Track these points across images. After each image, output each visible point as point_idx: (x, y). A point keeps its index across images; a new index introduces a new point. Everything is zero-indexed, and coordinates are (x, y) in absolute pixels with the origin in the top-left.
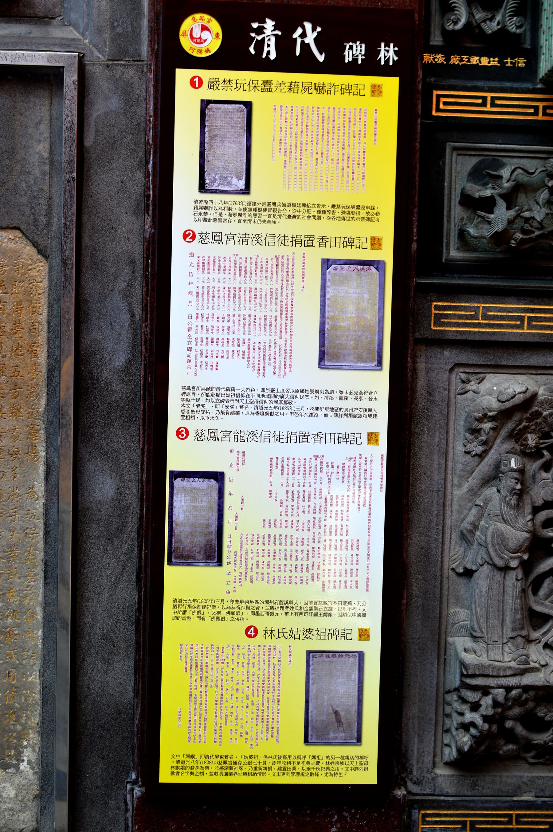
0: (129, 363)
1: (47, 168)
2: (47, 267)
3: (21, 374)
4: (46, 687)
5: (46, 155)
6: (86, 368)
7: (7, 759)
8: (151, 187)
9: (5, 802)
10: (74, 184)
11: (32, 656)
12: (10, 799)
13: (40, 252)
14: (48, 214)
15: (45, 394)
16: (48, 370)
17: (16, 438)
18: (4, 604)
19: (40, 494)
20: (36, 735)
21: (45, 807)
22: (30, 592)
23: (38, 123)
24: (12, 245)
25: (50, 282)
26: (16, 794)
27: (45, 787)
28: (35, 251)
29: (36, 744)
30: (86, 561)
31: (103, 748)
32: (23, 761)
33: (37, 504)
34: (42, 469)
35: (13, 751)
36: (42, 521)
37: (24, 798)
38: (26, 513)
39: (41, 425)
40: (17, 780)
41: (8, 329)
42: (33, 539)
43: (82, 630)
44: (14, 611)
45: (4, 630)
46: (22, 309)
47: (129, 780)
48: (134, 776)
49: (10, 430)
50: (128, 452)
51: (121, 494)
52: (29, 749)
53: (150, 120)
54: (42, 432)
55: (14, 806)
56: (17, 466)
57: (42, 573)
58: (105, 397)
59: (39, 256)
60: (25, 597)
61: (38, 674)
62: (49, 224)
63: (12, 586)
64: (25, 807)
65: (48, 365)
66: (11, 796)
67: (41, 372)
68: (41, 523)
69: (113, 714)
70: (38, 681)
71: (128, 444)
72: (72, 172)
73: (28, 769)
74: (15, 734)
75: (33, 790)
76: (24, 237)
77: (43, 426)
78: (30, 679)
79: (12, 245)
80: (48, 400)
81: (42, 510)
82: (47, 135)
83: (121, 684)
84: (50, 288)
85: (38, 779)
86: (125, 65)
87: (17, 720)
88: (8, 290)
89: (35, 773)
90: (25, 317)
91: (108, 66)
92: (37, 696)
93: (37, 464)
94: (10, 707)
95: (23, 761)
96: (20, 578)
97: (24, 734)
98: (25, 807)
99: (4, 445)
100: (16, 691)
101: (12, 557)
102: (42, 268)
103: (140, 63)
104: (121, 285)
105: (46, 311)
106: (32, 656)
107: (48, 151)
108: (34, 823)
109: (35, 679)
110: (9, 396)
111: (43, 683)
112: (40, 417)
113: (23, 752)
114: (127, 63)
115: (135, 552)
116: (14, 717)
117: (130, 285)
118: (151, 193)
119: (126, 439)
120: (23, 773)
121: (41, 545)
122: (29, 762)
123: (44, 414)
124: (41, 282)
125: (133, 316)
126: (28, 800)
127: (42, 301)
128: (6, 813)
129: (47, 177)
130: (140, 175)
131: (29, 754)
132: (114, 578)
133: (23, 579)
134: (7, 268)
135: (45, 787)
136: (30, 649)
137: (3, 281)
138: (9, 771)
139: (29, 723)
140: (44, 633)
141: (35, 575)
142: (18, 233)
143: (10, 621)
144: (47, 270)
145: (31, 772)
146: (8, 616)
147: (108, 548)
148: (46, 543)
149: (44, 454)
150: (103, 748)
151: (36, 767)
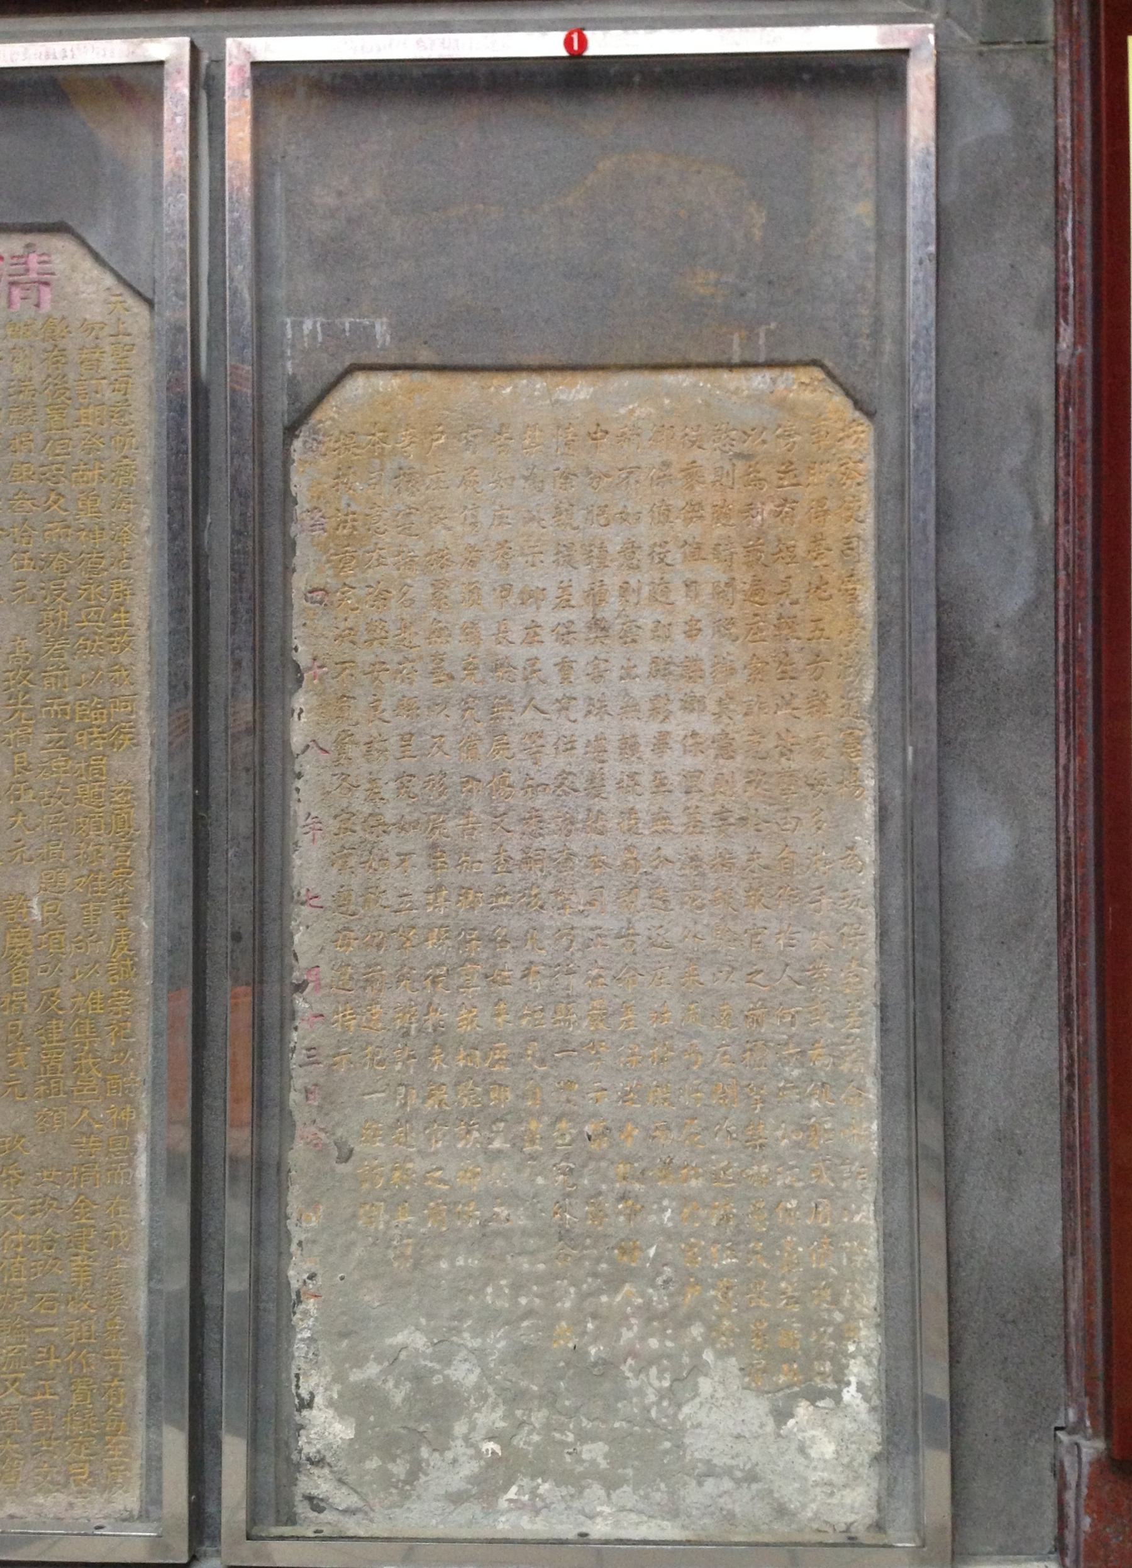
0: (1034, 605)
1: (871, 248)
2: (872, 434)
3: (826, 633)
4: (890, 1236)
5: (869, 223)
6: (949, 617)
7: (818, 1380)
8: (1071, 270)
9: (815, 1468)
10: (931, 267)
11: (859, 1173)
12: (825, 1461)
13: (858, 405)
14: (876, 334)
15: (873, 670)
16: (880, 623)
17: (819, 753)
18: (804, 1070)
19: (867, 860)
20: (873, 1331)
21: (895, 1479)
22: (853, 1047)
23: (854, 166)
24: (807, 395)
25: (879, 456)
26: (837, 1452)
27: (896, 1438)
28: (849, 404)
29: (873, 1350)
30: (958, 987)
31: (1006, 1359)
32: (848, 1384)
33: (863, 877)
34: (869, 811)
35: (828, 1363)
36: (872, 910)
37: (853, 1460)
38: (842, 895)
39: (866, 729)
40: (836, 1424)
41: (801, 551)
42: (855, 945)
43: (956, 1121)
44: (823, 1084)
45: (804, 1122)
46: (826, 512)
47: (1060, 1423)
48: (1072, 1415)
49: (808, 741)
50: (1035, 775)
51: (1022, 856)
52: (860, 1360)
53: (1065, 147)
54: (869, 741)
55: (833, 1477)
56: (823, 806)
57: (874, 1012)
58: (987, 672)
59: (857, 414)
60: (841, 1057)
61: (872, 1208)
62: (876, 352)
63: (817, 1036)
64: (856, 1478)
65: (879, 613)
66: (827, 1457)
67: (864, 628)
68: (870, 916)
69: (1023, 1290)
70: (872, 1222)
71: (1033, 759)
72: (927, 244)
73: (858, 1401)
74: (830, 1330)
75: (869, 1443)
76: (828, 380)
77: (870, 731)
78: (857, 1219)
79: (807, 395)
80: (880, 682)
81: (871, 889)
82: (870, 185)
83: (1037, 1229)
84: (879, 472)
85: (880, 1422)
86: (1011, 51)
87: (836, 1301)
88: (802, 479)
89: (873, 1409)
90: (832, 528)
91: (981, 54)
92: (872, 1253)
93: (860, 803)
94: (820, 1275)
95: (848, 1384)
96: (832, 1021)
97: (849, 1330)
98: (856, 1478)
99: (798, 767)
100: (831, 1244)
101: (816, 980)
102: (862, 436)
103: (1038, 46)
104: (1013, 459)
105: (872, 515)
106: (859, 1173)
107: (872, 215)
108: (873, 1512)
109: (869, 1219)
110: (805, 676)
111: (885, 1228)
112: (864, 714)
113: (847, 1366)
114: (1017, 47)
115: (1055, 968)
116: (827, 1294)
117: (1033, 457)
118: (1071, 281)
119: (1029, 749)
120: (849, 1410)
121: (872, 956)
122: (861, 1387)
123: (871, 706)
124: (861, 461)
125: (1037, 516)
126: (861, 1465)
127: (864, 496)
128: (818, 1489)
129: (872, 265)
130: (1046, 253)
131: (858, 1371)
132: (1014, 1019)
133: (838, 1023)
134: (797, 438)
135: (896, 1438)
136: (855, 1159)
137: (791, 463)
138: (820, 1404)
139: (858, 1306)
140: (883, 1127)
141: (862, 1014)
142: (818, 373)
143: (815, 1104)
144: (871, 440)
145: (863, 1407)
146: (811, 1095)
147: (1002, 961)
148: (882, 951)
149: (872, 783)
150: (1006, 1359)
151: (875, 1397)
